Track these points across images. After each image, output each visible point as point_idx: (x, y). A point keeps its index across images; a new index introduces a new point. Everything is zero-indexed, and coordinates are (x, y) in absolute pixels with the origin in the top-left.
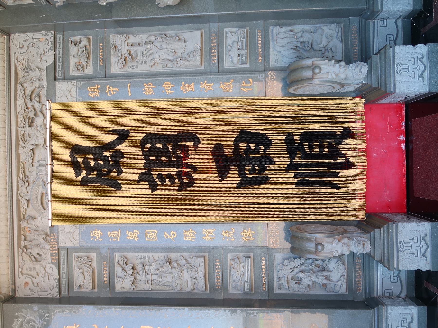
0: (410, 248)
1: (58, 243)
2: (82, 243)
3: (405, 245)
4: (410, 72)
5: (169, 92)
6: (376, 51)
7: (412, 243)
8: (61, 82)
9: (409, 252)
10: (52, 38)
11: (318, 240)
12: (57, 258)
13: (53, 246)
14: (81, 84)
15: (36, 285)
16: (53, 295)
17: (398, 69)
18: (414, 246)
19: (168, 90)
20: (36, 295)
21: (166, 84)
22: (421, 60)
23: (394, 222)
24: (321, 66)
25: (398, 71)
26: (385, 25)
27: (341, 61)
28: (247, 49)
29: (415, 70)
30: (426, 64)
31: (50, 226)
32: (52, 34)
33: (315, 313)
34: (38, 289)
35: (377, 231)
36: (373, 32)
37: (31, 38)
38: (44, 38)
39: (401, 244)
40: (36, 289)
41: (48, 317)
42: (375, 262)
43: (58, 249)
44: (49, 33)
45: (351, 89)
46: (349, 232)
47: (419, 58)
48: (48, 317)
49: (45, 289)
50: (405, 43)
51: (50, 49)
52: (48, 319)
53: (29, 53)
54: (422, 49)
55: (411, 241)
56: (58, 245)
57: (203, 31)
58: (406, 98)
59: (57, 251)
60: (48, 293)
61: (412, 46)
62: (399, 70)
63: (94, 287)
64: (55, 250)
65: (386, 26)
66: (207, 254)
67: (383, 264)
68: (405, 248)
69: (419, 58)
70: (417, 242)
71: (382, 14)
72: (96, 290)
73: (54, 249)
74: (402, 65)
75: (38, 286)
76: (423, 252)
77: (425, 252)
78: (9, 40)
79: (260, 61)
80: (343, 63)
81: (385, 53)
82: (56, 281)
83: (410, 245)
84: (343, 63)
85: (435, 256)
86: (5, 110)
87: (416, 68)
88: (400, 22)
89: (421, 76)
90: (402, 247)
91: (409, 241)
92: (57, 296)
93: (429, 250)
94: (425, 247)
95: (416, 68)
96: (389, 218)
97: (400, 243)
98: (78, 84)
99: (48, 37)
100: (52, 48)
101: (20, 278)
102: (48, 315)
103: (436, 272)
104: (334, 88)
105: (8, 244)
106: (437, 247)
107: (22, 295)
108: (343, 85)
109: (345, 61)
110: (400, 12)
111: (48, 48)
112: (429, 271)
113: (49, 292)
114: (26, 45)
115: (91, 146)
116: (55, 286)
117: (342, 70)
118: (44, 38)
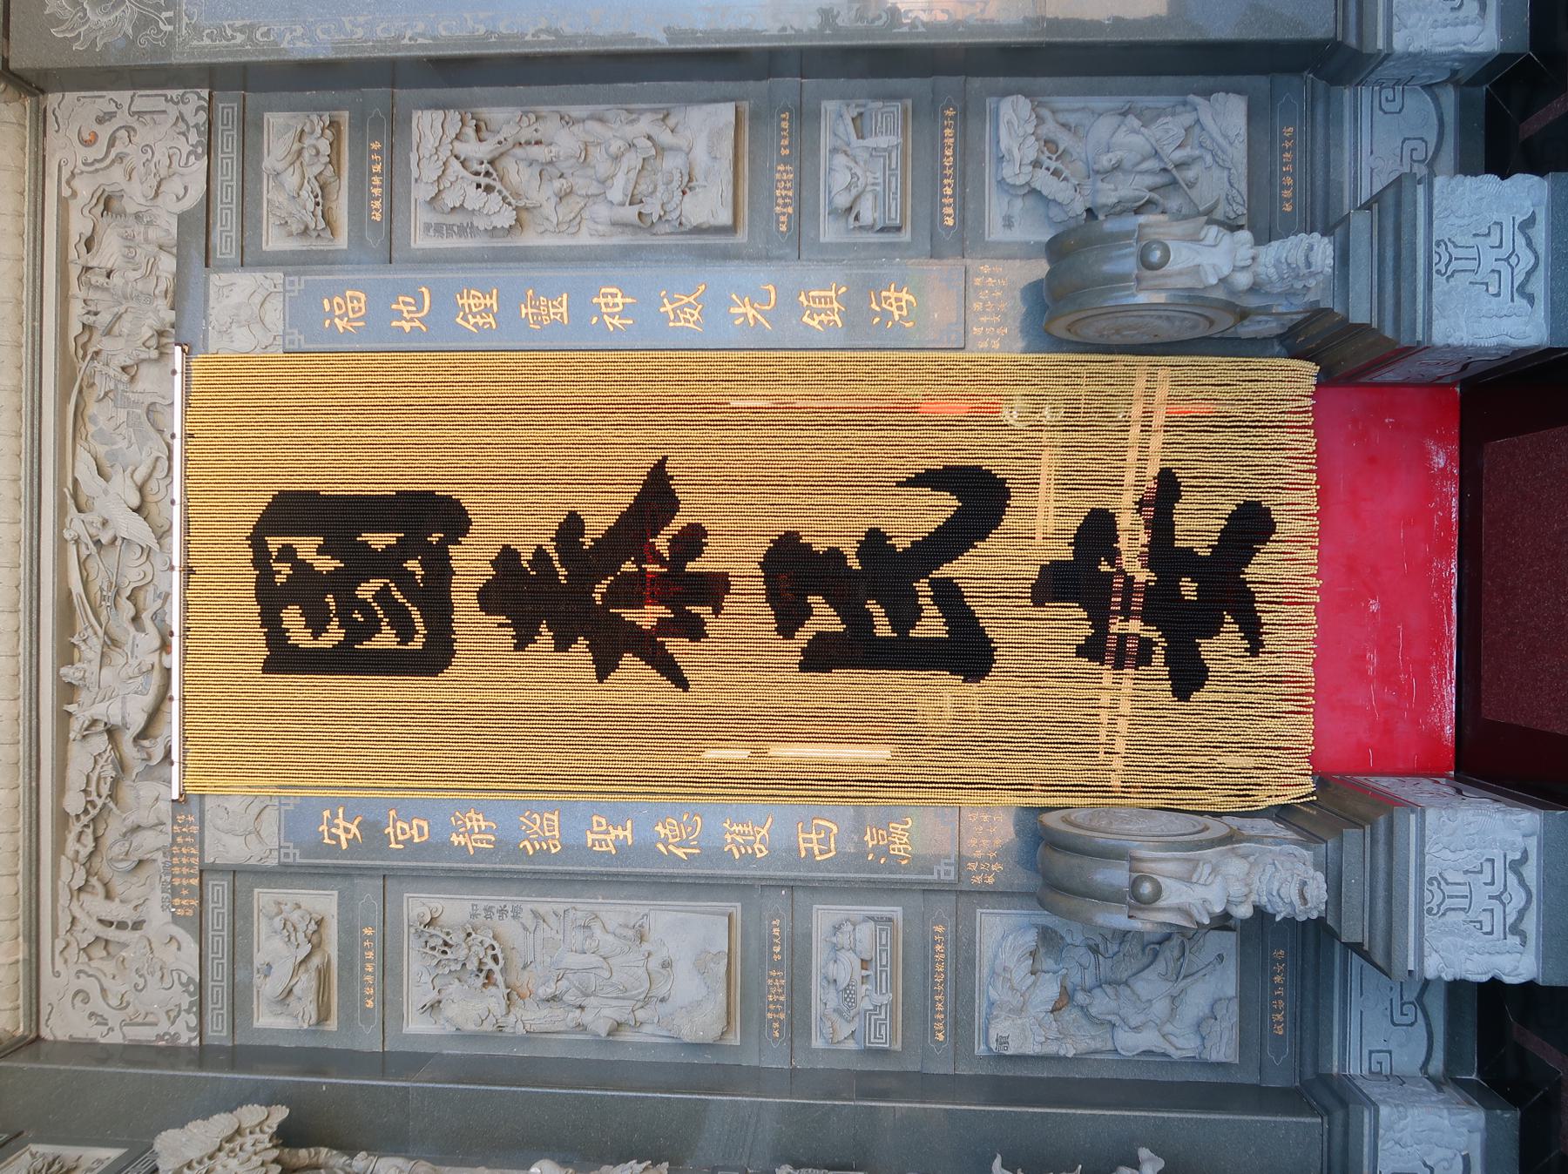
0: (1473, 265)
1: (202, 850)
2: (287, 855)
3: (1448, 889)
4: (1486, 272)
5: (616, 322)
6: (1365, 196)
7: (1471, 885)
8: (226, 277)
9: (1462, 916)
10: (203, 116)
11: (1147, 230)
12: (195, 903)
13: (184, 861)
14: (299, 283)
15: (115, 1002)
16: (176, 1036)
17: (1433, 898)
18: (1489, 261)
19: (612, 315)
20: (116, 1038)
21: (605, 295)
22: (1516, 867)
23: (1411, 806)
24: (1172, 245)
25: (1434, 904)
26: (1395, 107)
27: (1241, 227)
28: (894, 990)
29: (1496, 904)
30: (1534, 891)
31: (175, 796)
32: (200, 98)
33: (1118, 22)
34: (121, 1015)
35: (1352, 835)
36: (1356, 178)
37: (126, 107)
38: (173, 111)
39: (1434, 888)
40: (114, 1018)
41: (169, 21)
42: (1337, 945)
43: (201, 871)
44: (192, 97)
45: (1269, 327)
46: (1250, 839)
47: (1509, 858)
48: (169, 21)
49: (150, 1019)
50: (1465, 167)
51: (195, 153)
52: (170, 28)
53: (116, 278)
54: (1526, 193)
55: (1470, 878)
56: (202, 858)
57: (745, 106)
58: (1465, 367)
59: (195, 882)
60: (161, 1029)
61: (1496, 178)
62: (1437, 900)
63: (323, 1017)
64: (189, 876)
65: (1390, 1052)
66: (745, 240)
67: (1366, 956)
68: (1454, 265)
69: (1509, 858)
70: (1500, 246)
71: (1388, 64)
72: (332, 1025)
73: (185, 871)
74: (1456, 246)
75: (123, 1007)
76: (1510, 920)
77: (1522, 914)
78: (40, 120)
79: (941, 1037)
80: (1245, 235)
81: (1398, 204)
82: (192, 988)
83: (1473, 253)
84: (1245, 235)
85: (1555, 940)
86: (22, 194)
87: (1499, 898)
88: (1449, 97)
89: (1515, 929)
90: (1445, 259)
91: (1472, 242)
92: (191, 1040)
93: (1541, 272)
94: (1527, 259)
95: (1499, 898)
96: (1392, 791)
97: (1438, 245)
98: (292, 283)
99: (188, 110)
100: (200, 150)
101: (57, 974)
102: (171, 14)
103: (1551, 990)
104: (1212, 323)
105: (17, 631)
106: (1567, 901)
107: (62, 1035)
108: (1244, 315)
109: (1251, 229)
110: (1455, 60)
111: (186, 149)
112: (1530, 985)
113: (164, 1026)
114: (105, 132)
115: (326, 489)
116: (185, 1006)
117: (1237, 889)
118: (173, 111)
